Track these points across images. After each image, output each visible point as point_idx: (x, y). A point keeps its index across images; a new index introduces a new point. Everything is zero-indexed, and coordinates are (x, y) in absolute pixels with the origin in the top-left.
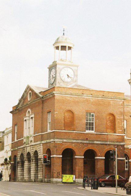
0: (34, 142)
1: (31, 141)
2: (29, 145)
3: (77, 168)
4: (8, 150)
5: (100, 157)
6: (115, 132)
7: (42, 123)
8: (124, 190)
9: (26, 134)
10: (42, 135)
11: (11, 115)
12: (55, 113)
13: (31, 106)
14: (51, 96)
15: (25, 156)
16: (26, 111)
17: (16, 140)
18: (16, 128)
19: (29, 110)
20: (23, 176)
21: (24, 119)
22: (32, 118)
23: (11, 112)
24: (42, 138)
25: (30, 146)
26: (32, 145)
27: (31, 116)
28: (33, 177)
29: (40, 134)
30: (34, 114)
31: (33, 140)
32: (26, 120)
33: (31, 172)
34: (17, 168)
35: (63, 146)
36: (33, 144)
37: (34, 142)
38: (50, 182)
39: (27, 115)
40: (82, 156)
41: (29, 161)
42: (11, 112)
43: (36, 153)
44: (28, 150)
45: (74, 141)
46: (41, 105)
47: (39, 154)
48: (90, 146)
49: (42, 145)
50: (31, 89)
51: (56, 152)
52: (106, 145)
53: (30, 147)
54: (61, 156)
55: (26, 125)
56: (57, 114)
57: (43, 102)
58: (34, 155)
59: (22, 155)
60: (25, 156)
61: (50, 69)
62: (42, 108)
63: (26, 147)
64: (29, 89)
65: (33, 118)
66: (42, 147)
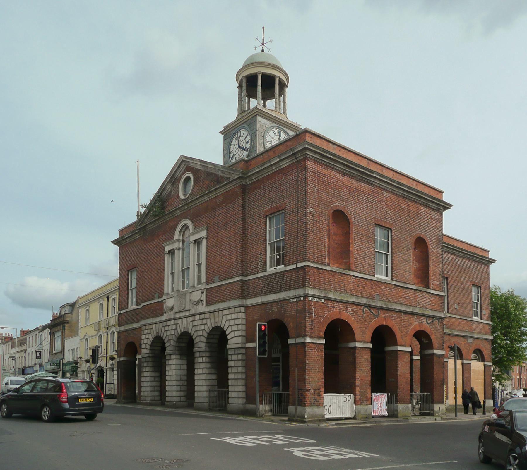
0: (208, 304)
1: (197, 303)
2: (188, 313)
3: (358, 375)
4: (111, 324)
5: (363, 343)
6: (427, 286)
7: (244, 250)
8: (6, 334)
10: (243, 283)
11: (116, 248)
12: (308, 210)
13: (197, 213)
16: (174, 228)
17: (132, 306)
19: (189, 223)
21: (167, 249)
22: (197, 242)
23: (115, 242)
24: (244, 291)
28: (173, 390)
29: (237, 279)
30: (207, 229)
31: (204, 297)
34: (140, 377)
35: (328, 312)
36: (202, 308)
37: (208, 304)
39: (177, 235)
40: (368, 342)
42: (115, 242)
44: (183, 325)
46: (240, 198)
48: (383, 315)
49: (242, 309)
50: (189, 169)
51: (311, 329)
53: (191, 319)
54: (323, 341)
57: (245, 190)
58: (207, 338)
62: (244, 207)
65: (204, 242)
66: (242, 315)
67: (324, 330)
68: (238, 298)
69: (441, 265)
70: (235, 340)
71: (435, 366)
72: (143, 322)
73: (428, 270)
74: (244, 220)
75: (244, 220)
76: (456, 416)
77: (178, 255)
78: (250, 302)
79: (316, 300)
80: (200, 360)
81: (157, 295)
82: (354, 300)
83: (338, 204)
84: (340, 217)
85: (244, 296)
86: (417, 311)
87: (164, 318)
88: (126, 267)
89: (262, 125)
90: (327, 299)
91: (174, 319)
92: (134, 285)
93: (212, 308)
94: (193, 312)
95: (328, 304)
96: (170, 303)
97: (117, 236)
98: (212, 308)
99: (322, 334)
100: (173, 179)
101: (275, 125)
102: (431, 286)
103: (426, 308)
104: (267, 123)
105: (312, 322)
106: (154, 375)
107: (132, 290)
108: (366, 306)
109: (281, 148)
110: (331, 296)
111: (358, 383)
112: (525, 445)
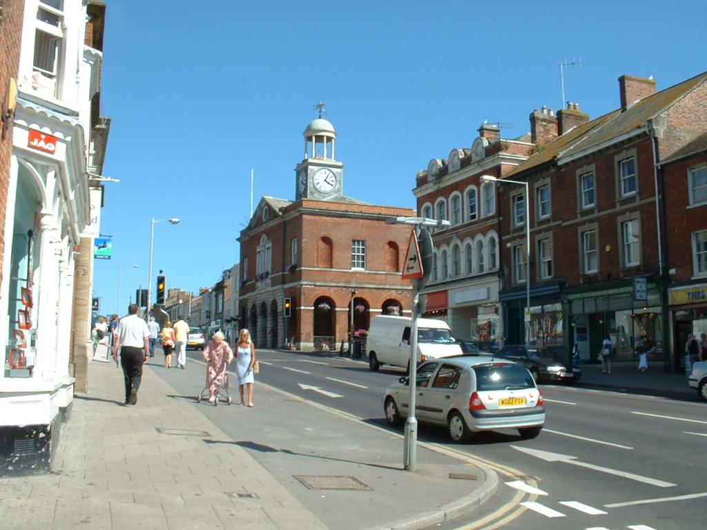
23: (238, 240)
25: (266, 292)
27: (267, 247)
37: (272, 286)
42: (238, 240)
43: (274, 303)
54: (313, 308)
56: (305, 242)
59: (254, 306)
63: (260, 294)
67: (313, 302)
68: (279, 284)
71: (694, 328)
72: (248, 295)
74: (284, 240)
75: (284, 240)
78: (286, 286)
79: (308, 286)
82: (334, 284)
83: (324, 234)
84: (327, 241)
85: (284, 282)
86: (387, 287)
88: (244, 255)
89: (312, 170)
90: (315, 285)
91: (260, 294)
95: (317, 288)
97: (239, 236)
99: (312, 304)
101: (320, 168)
103: (396, 285)
104: (316, 168)
105: (305, 298)
106: (82, 301)
108: (344, 287)
110: (318, 284)
111: (337, 330)
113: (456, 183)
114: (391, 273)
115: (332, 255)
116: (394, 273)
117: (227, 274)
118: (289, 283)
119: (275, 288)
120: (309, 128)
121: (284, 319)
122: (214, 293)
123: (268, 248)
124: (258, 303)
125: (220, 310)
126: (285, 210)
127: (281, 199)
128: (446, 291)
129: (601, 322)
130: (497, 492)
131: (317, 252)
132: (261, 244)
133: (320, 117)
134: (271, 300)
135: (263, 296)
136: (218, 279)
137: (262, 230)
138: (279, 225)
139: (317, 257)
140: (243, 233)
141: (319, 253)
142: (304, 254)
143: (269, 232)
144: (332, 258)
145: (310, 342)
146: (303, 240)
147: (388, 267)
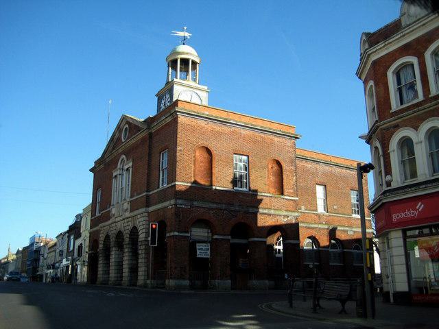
6: (282, 194)
7: (149, 175)
9: (115, 198)
14: (169, 120)
15: (113, 240)
18: (99, 194)
20: (109, 274)
23: (92, 170)
25: (124, 219)
26: (127, 218)
27: (126, 167)
32: (116, 176)
33: (111, 268)
37: (132, 211)
38: (162, 286)
41: (120, 246)
43: (134, 231)
44: (120, 226)
45: (215, 206)
47: (139, 233)
49: (146, 214)
50: (127, 122)
52: (269, 215)
55: (115, 185)
56: (180, 150)
59: (107, 237)
60: (113, 240)
61: (160, 97)
63: (115, 222)
64: (124, 118)
69: (294, 178)
70: (142, 236)
72: (101, 225)
73: (282, 181)
74: (150, 155)
75: (150, 155)
76: (291, 306)
77: (119, 177)
80: (101, 255)
81: (135, 194)
85: (148, 205)
87: (110, 222)
91: (115, 222)
92: (165, 165)
93: (132, 214)
94: (123, 217)
96: (114, 211)
98: (132, 214)
100: (119, 128)
102: (286, 194)
107: (163, 170)
109: (108, 155)
112: (260, 319)
113: (427, 34)
114: (276, 196)
115: (212, 164)
116: (276, 196)
117: (79, 217)
118: (155, 204)
119: (136, 212)
120: (175, 53)
121: (147, 249)
122: (67, 235)
123: (127, 169)
124: (113, 233)
125: (71, 248)
126: (149, 121)
127: (143, 110)
128: (130, 285)
129: (286, 276)
130: (23, 262)
131: (195, 165)
132: (118, 167)
133: (184, 44)
134: (129, 228)
135: (119, 224)
136: (71, 221)
137: (120, 151)
138: (143, 140)
139: (194, 171)
140: (98, 163)
141: (197, 166)
142: (179, 166)
143: (128, 153)
144: (212, 173)
145: (184, 279)
146: (178, 149)
147: (272, 190)
